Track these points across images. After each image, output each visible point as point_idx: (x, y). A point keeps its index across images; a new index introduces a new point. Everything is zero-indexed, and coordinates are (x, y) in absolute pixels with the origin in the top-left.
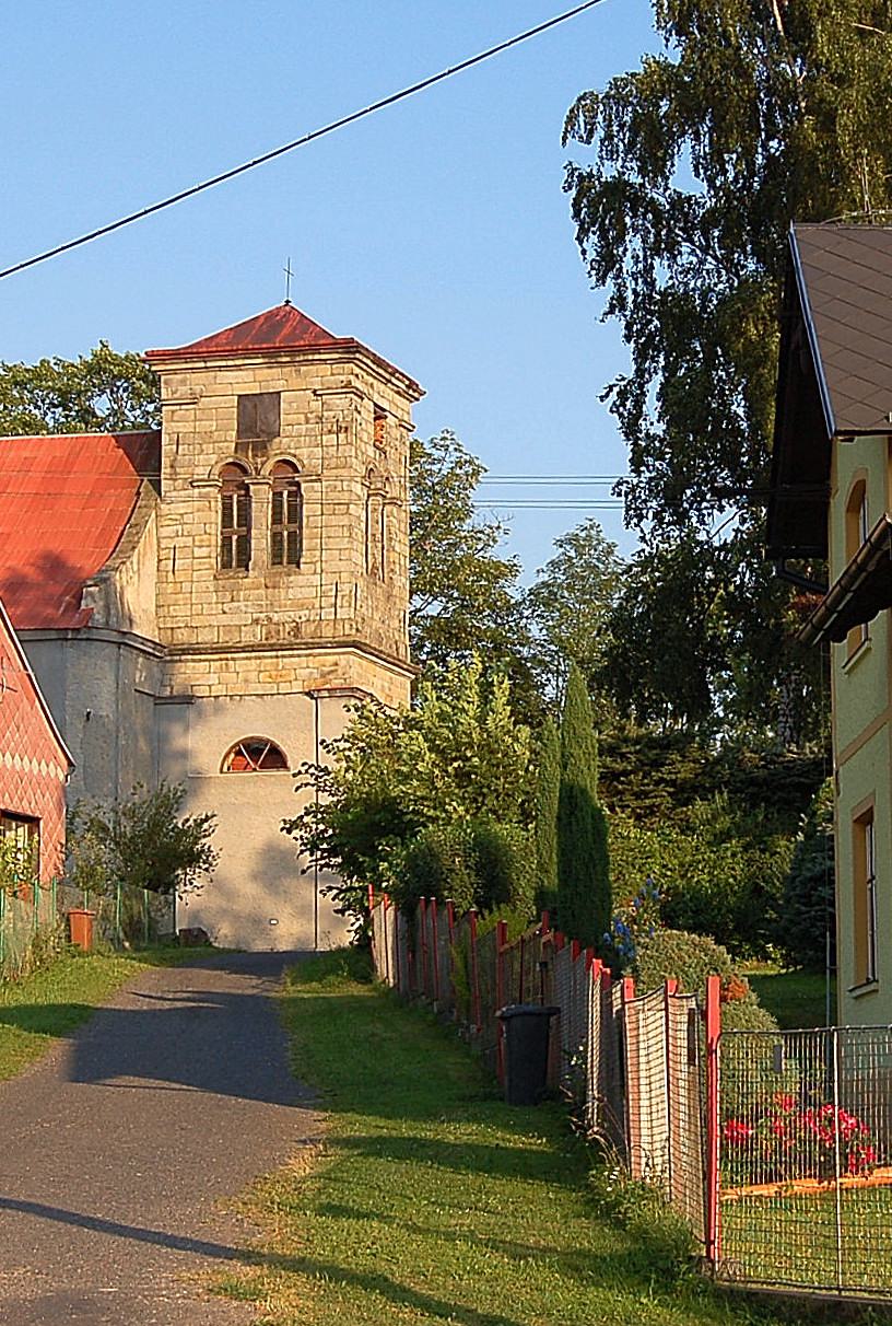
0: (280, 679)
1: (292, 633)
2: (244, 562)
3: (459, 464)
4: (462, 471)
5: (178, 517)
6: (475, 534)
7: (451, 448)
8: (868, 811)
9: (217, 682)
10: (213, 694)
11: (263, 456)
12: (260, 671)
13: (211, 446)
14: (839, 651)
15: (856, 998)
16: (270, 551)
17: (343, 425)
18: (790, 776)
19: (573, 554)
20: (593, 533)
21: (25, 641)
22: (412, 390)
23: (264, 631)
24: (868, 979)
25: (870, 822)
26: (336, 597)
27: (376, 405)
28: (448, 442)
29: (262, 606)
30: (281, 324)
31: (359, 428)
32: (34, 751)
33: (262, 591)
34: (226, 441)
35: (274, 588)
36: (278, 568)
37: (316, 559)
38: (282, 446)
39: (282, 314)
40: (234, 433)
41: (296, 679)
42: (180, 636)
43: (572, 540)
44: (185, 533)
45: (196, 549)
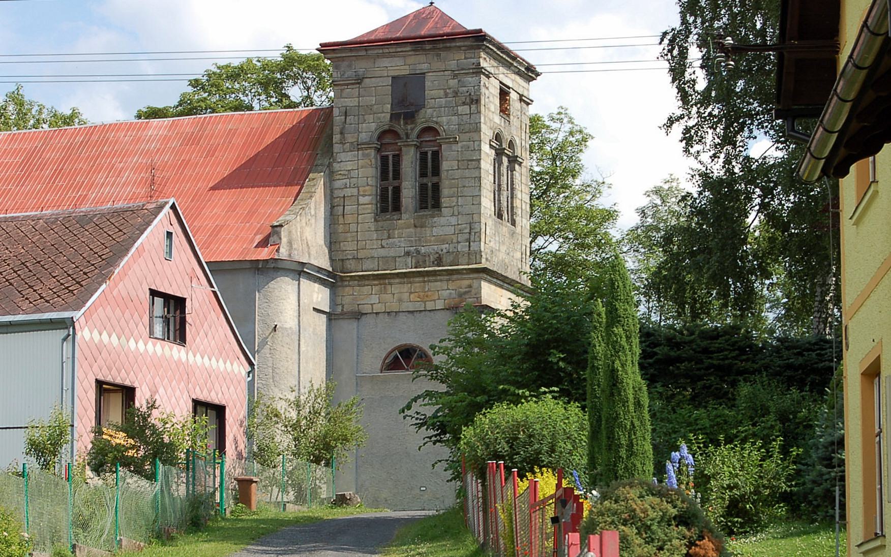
0: (426, 299)
1: (436, 262)
2: (397, 207)
3: (571, 133)
4: (574, 139)
5: (347, 173)
6: (586, 188)
7: (565, 120)
8: (876, 358)
9: (378, 302)
10: (374, 312)
11: (412, 124)
12: (411, 293)
13: (372, 116)
14: (848, 185)
15: (865, 553)
16: (418, 198)
17: (474, 98)
18: (822, 361)
19: (659, 202)
20: (674, 184)
21: (213, 270)
22: (529, 73)
23: (414, 261)
24: (876, 534)
25: (878, 374)
26: (470, 233)
27: (501, 82)
28: (563, 116)
29: (412, 241)
30: (426, 19)
31: (487, 100)
32: (221, 353)
33: (412, 230)
34: (383, 112)
35: (422, 227)
36: (427, 212)
37: (454, 204)
38: (427, 115)
39: (427, 12)
40: (389, 106)
41: (439, 299)
42: (349, 266)
43: (657, 191)
44: (352, 185)
45: (360, 198)
